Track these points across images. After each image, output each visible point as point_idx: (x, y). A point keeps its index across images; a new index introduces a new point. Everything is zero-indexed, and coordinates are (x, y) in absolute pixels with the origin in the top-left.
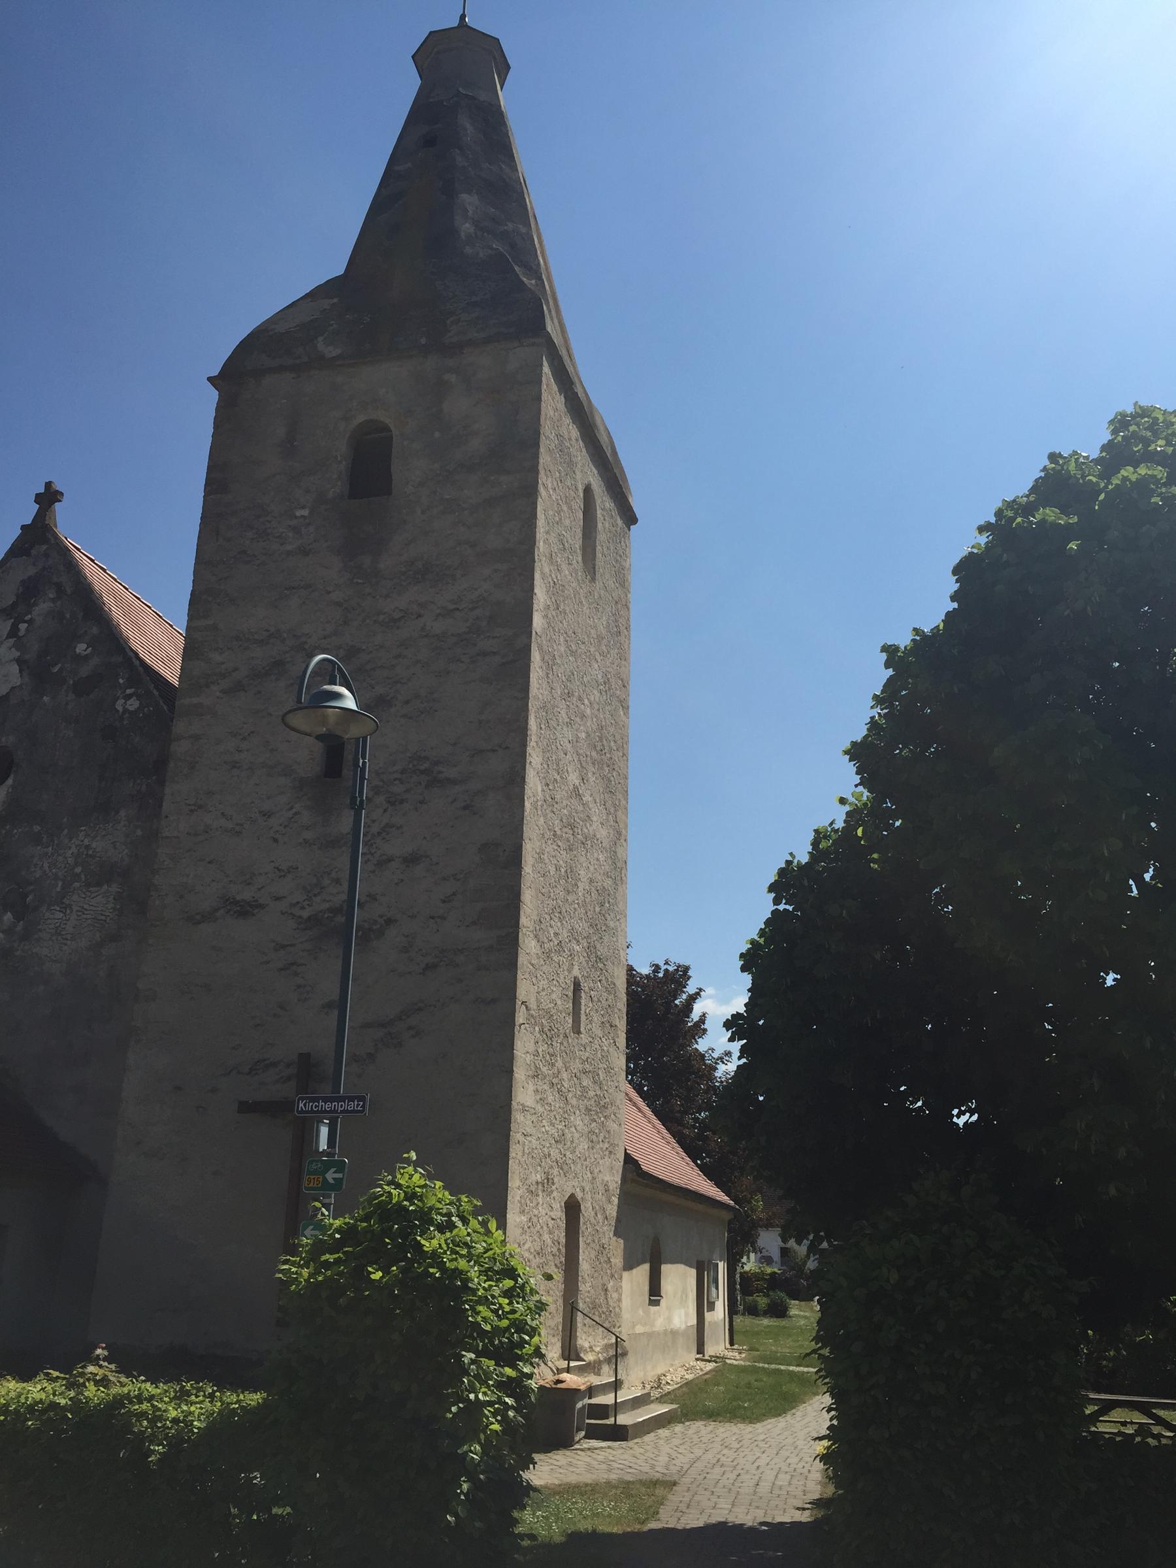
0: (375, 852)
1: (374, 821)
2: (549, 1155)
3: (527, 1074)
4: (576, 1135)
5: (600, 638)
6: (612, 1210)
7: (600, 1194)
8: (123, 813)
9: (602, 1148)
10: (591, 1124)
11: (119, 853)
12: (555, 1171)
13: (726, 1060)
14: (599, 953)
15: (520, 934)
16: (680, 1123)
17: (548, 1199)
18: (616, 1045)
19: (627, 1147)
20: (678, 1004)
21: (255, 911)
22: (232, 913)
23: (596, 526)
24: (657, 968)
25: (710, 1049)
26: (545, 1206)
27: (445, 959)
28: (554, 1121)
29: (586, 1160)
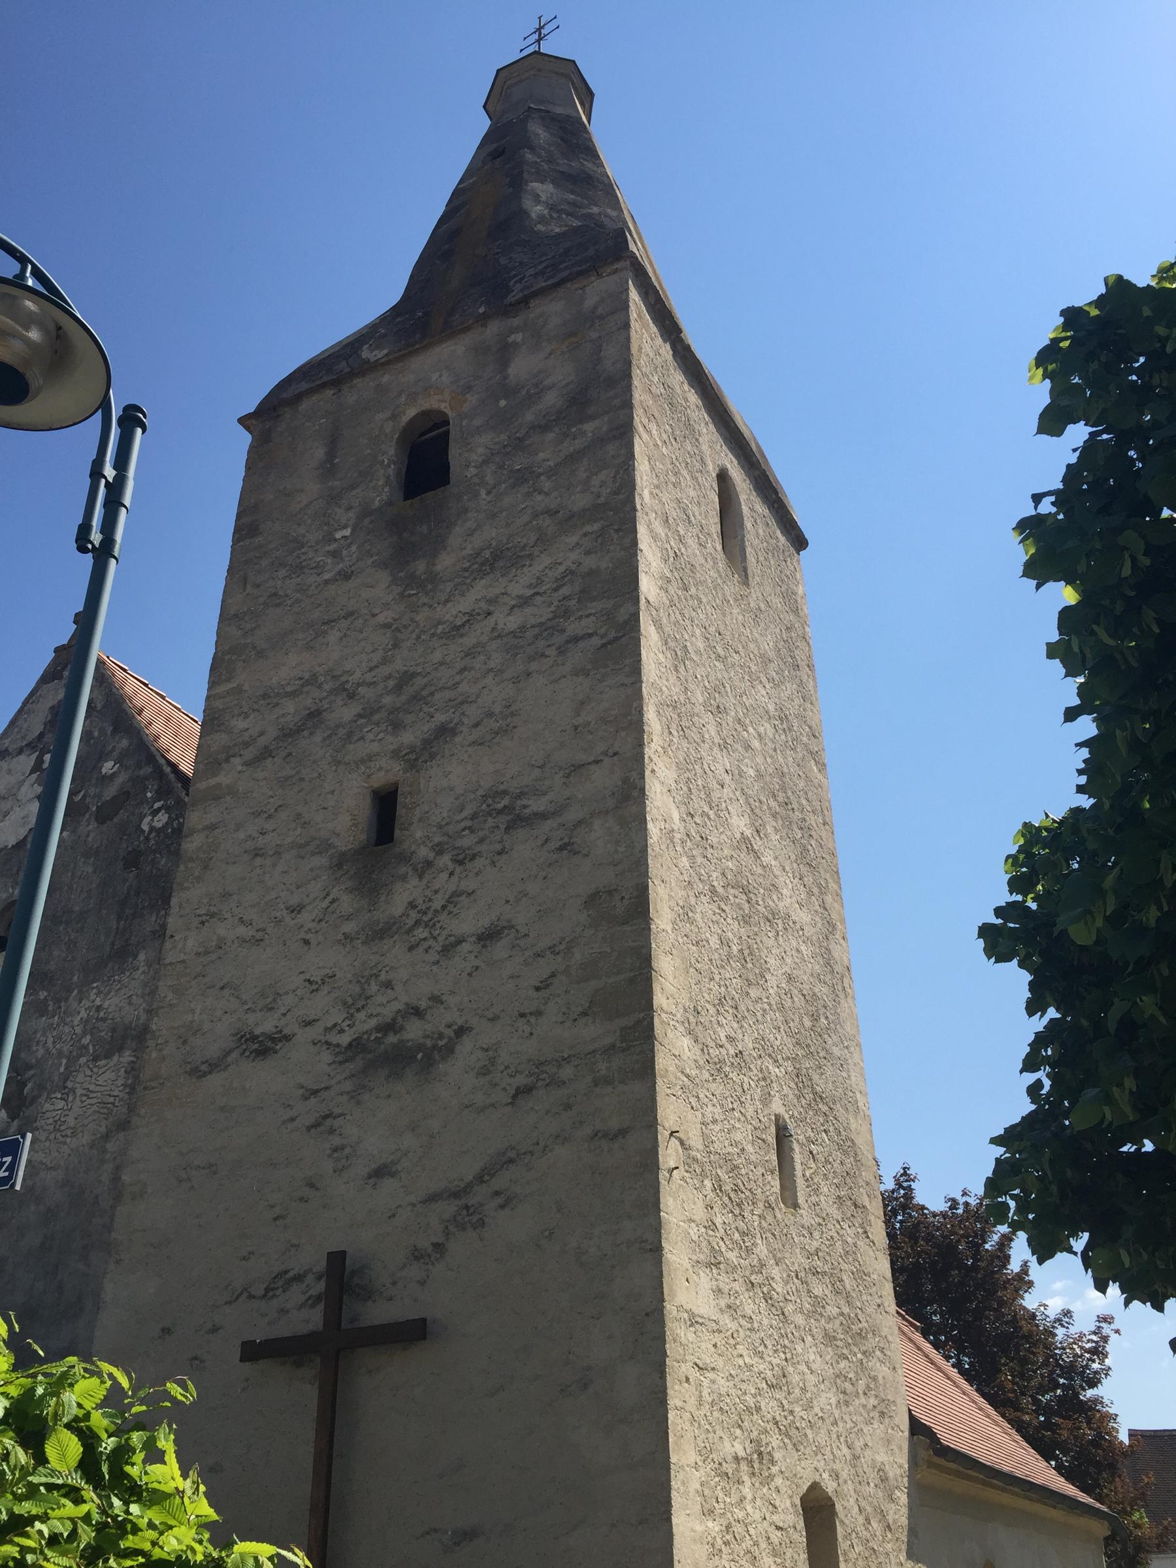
0: (439, 935)
1: (436, 892)
2: (758, 1409)
3: (694, 1258)
4: (812, 1379)
5: (766, 661)
6: (899, 1512)
7: (872, 1485)
8: (142, 957)
9: (864, 1406)
10: (838, 1363)
11: (135, 1010)
12: (775, 1440)
13: (1067, 1323)
14: (818, 1089)
15: (656, 1021)
16: (1017, 1408)
17: (765, 1490)
18: (868, 1237)
19: (911, 1407)
20: (990, 1248)
21: (278, 1047)
22: (247, 1053)
23: (742, 524)
24: (954, 1203)
25: (1040, 1306)
26: (759, 1502)
27: (544, 1076)
28: (761, 1348)
29: (835, 1423)
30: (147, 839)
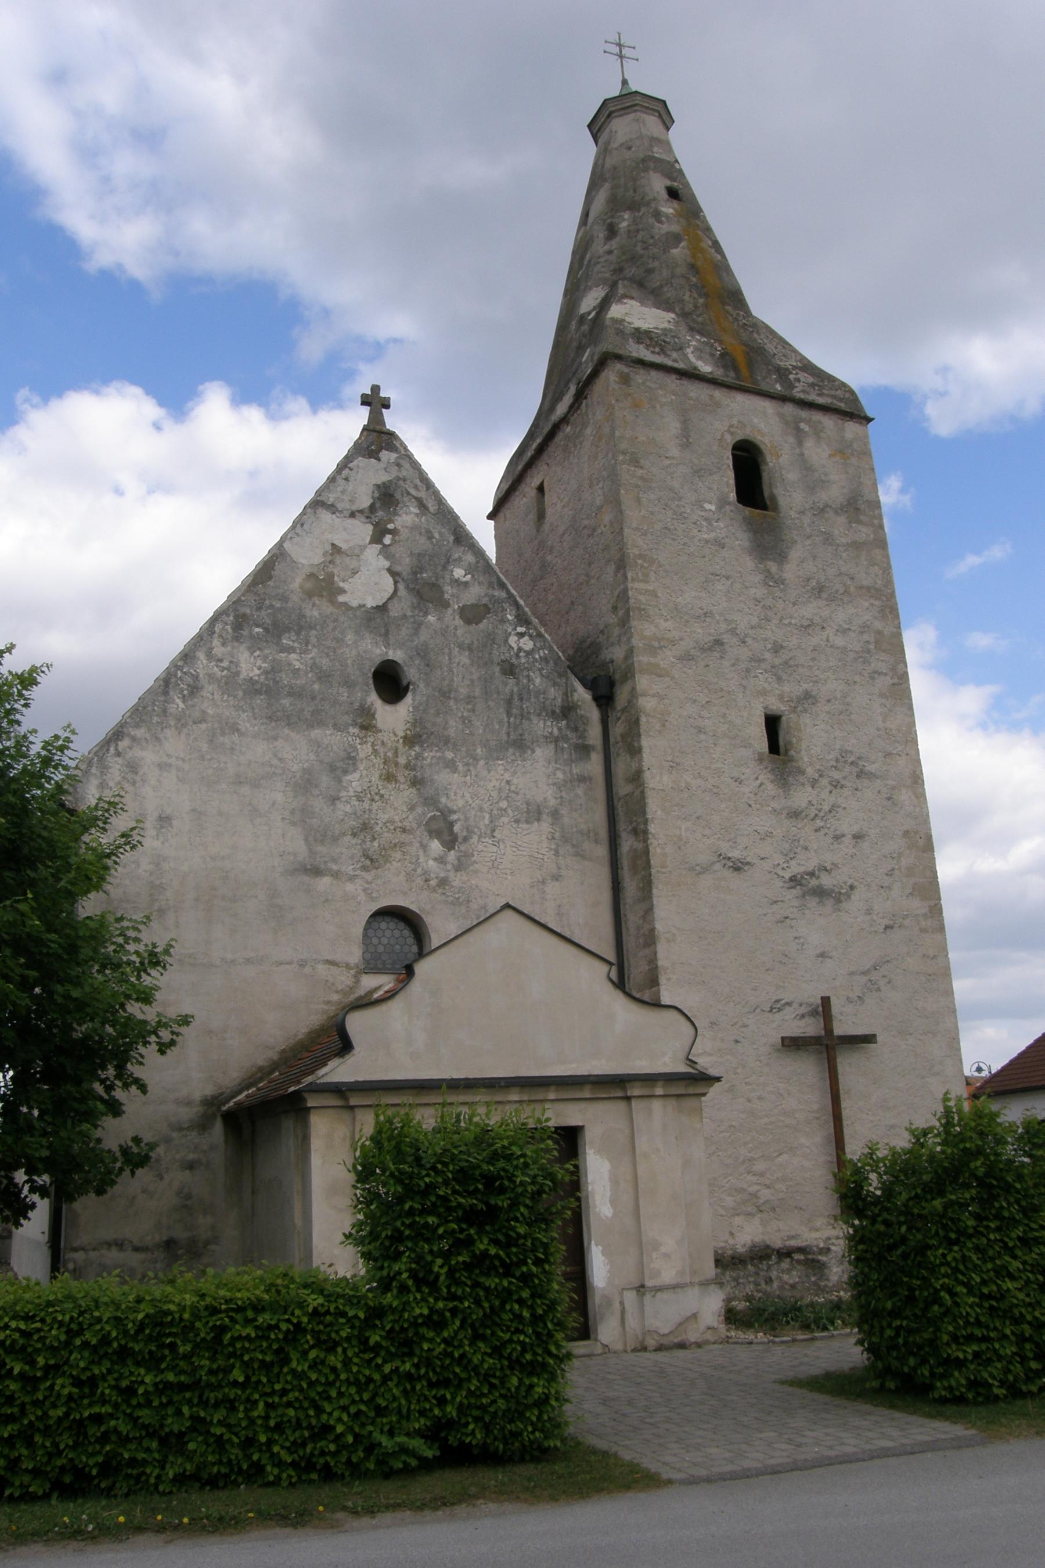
30: (517, 656)
